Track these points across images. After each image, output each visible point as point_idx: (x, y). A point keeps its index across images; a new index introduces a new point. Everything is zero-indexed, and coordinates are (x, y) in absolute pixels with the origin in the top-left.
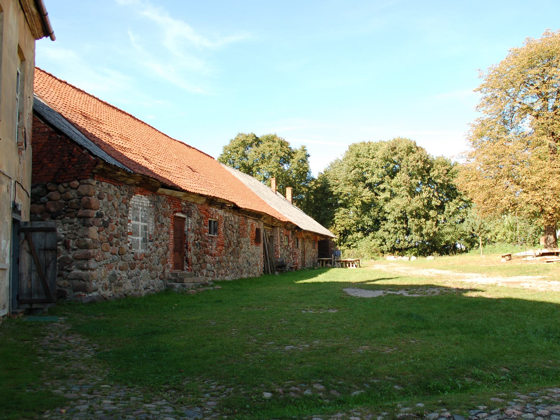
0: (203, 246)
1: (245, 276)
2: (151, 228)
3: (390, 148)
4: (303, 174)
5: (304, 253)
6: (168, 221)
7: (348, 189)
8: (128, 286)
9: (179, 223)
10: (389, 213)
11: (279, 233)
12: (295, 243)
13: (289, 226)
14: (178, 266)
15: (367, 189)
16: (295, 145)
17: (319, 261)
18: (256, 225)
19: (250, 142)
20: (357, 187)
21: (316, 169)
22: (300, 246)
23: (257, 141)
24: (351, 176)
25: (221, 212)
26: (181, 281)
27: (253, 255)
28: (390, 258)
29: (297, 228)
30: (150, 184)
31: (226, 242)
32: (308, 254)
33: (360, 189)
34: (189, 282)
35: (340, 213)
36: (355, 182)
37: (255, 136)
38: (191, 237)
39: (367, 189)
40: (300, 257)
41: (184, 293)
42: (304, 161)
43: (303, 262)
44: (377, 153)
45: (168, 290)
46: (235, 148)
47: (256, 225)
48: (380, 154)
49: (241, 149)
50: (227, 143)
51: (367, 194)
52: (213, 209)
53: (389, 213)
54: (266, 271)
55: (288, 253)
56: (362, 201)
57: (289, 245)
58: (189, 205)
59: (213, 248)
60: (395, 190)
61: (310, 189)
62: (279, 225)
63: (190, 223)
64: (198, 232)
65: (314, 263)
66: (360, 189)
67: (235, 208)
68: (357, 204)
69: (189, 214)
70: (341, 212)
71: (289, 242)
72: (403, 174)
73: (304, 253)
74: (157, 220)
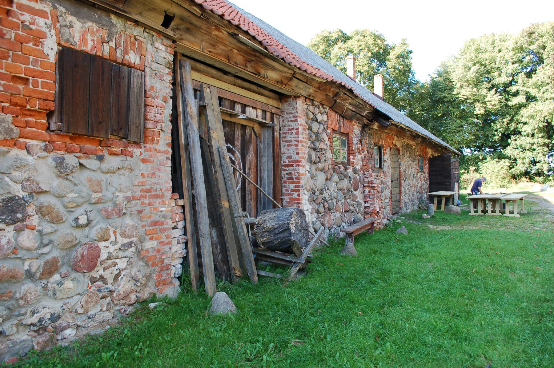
3: (525, 34)
5: (397, 181)
10: (525, 124)
12: (371, 157)
13: (347, 105)
15: (493, 91)
16: (392, 39)
17: (431, 198)
19: (334, 38)
21: (423, 74)
22: (387, 165)
24: (471, 74)
32: (405, 184)
33: (484, 92)
36: (477, 83)
40: (387, 193)
43: (396, 203)
44: (506, 44)
46: (315, 45)
48: (511, 44)
53: (525, 124)
55: (345, 184)
57: (349, 163)
60: (533, 92)
62: (304, 90)
65: (421, 201)
68: (479, 112)
71: (350, 152)
72: (548, 67)
73: (397, 181)
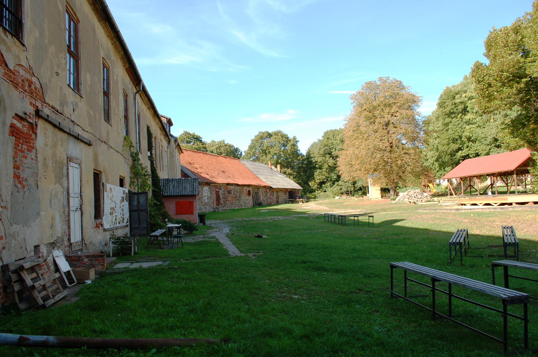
0: (226, 198)
1: (243, 207)
2: (209, 195)
4: (295, 153)
6: (214, 192)
7: (320, 159)
8: (204, 210)
9: (217, 193)
11: (261, 192)
14: (218, 205)
15: (331, 158)
16: (291, 137)
18: (248, 189)
20: (325, 157)
21: (303, 149)
23: (270, 135)
25: (232, 187)
26: (218, 209)
27: (249, 200)
28: (344, 197)
29: (271, 187)
30: (208, 183)
31: (234, 196)
34: (220, 209)
35: (317, 173)
37: (268, 132)
38: (221, 196)
39: (331, 158)
41: (218, 212)
42: (294, 145)
45: (215, 211)
47: (248, 189)
49: (260, 141)
50: (253, 138)
51: (331, 162)
52: (229, 186)
54: (254, 206)
56: (329, 165)
58: (220, 187)
59: (229, 199)
61: (299, 160)
63: (221, 192)
64: (224, 194)
66: (327, 159)
67: (238, 185)
69: (220, 189)
70: (318, 172)
74: (211, 192)
